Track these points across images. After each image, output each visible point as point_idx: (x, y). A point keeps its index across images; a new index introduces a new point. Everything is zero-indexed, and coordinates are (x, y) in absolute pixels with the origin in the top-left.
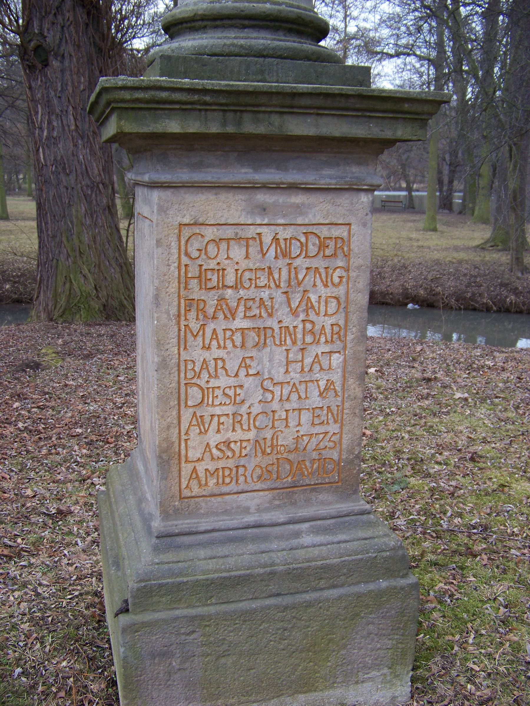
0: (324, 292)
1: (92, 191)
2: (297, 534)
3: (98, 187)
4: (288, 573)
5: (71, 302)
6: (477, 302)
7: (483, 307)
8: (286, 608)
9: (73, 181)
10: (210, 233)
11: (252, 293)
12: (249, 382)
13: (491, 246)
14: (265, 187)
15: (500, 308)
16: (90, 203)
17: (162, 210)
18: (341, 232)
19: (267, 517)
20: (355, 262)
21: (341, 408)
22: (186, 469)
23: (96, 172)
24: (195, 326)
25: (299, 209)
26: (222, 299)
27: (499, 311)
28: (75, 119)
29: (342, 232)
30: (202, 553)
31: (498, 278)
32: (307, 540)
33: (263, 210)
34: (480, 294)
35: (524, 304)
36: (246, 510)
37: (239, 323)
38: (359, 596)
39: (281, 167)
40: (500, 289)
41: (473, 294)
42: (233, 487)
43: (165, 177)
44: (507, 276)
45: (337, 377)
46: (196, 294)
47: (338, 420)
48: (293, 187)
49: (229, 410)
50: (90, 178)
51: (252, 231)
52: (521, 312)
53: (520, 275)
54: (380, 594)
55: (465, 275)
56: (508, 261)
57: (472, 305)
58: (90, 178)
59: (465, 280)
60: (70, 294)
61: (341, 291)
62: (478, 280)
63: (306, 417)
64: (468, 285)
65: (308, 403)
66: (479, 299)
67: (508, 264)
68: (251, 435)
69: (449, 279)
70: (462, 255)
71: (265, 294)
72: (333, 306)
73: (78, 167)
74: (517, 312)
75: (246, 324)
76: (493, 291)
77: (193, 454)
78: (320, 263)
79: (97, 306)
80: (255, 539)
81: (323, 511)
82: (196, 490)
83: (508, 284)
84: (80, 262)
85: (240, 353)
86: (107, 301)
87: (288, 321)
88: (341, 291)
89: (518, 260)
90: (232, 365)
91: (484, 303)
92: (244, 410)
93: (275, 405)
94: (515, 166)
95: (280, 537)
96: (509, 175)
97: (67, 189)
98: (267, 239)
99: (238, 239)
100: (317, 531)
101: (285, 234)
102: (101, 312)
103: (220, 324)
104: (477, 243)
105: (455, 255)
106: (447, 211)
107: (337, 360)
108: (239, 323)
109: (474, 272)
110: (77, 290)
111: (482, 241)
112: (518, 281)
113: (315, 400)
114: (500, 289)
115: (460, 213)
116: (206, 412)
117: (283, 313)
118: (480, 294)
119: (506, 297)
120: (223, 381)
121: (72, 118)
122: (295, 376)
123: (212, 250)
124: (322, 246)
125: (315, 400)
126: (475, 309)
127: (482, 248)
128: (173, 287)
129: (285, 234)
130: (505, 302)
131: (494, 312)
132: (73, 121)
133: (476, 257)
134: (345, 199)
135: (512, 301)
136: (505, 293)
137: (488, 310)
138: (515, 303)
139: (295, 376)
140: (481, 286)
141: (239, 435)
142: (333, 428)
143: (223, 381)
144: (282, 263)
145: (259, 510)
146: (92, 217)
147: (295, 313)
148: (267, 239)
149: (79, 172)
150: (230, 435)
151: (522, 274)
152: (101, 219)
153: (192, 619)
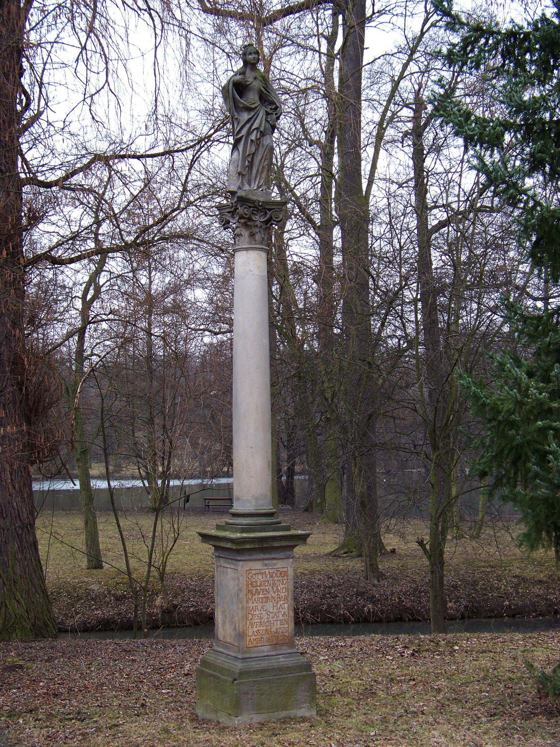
0: (282, 586)
1: (23, 531)
2: (279, 658)
3: (27, 527)
4: (278, 668)
5: (6, 623)
6: (334, 614)
7: (340, 619)
8: (278, 679)
9: (8, 524)
10: (253, 572)
11: (264, 587)
12: (264, 612)
13: (345, 553)
14: (267, 559)
15: (359, 619)
16: (21, 541)
17: (242, 567)
18: (285, 570)
19: (270, 654)
20: (289, 578)
21: (288, 619)
22: (248, 638)
23: (26, 515)
24: (250, 597)
25: (275, 564)
26: (257, 589)
27: (357, 622)
28: (11, 474)
29: (285, 570)
30: (254, 663)
31: (354, 587)
32: (282, 660)
33: (266, 565)
34: (336, 606)
35: (382, 612)
36: (264, 652)
37: (261, 596)
38: (299, 676)
39: (270, 554)
40: (356, 598)
41: (329, 606)
42: (260, 644)
43: (243, 558)
44: (362, 585)
45: (286, 610)
46: (250, 588)
47: (287, 623)
48: (274, 559)
49: (259, 621)
50: (21, 520)
51: (263, 571)
52: (380, 621)
53: (376, 582)
54: (304, 676)
55: (319, 586)
56: (363, 568)
57: (329, 617)
58: (21, 520)
59: (320, 592)
60: (6, 616)
61: (286, 586)
62: (333, 591)
63: (279, 622)
64: (323, 597)
65: (279, 619)
66: (336, 610)
67: (363, 571)
68: (265, 628)
69: (302, 592)
70: (314, 565)
71: (267, 588)
72: (284, 590)
73: (13, 512)
74: (376, 621)
75: (262, 596)
76: (350, 601)
77: (250, 634)
78: (280, 578)
79: (28, 626)
80: (267, 660)
81: (285, 652)
82: (251, 645)
83: (364, 593)
84: (14, 589)
85: (261, 604)
86: (35, 622)
87: (273, 595)
88: (286, 586)
89: (372, 567)
90: (259, 608)
91: (341, 614)
92: (262, 620)
93: (271, 619)
94: (360, 471)
95: (274, 659)
96: (355, 479)
97: (4, 530)
98: (267, 573)
99: (260, 573)
100: (284, 658)
101: (271, 571)
102: (32, 631)
103: (256, 596)
104: (329, 549)
105: (306, 565)
106: (289, 507)
107: (286, 605)
108: (261, 596)
109: (328, 583)
110: (12, 613)
111: (335, 547)
112: (374, 588)
113: (281, 618)
114: (356, 598)
115: (306, 510)
116: (253, 621)
117: (272, 593)
118: (336, 606)
119: (364, 606)
120: (257, 612)
121: (9, 473)
122: (275, 610)
123: (254, 576)
124: (281, 574)
125: (281, 618)
126: (332, 622)
127: (334, 555)
128: (245, 587)
129: (271, 571)
130: (363, 611)
131: (353, 623)
132: (9, 476)
133: (331, 566)
134: (286, 561)
135: (369, 610)
136: (362, 602)
137: (346, 621)
138: (373, 612)
139: (275, 610)
140: (337, 596)
141: (261, 628)
142: (286, 626)
143: (257, 612)
144: (271, 579)
145: (267, 652)
146: (23, 552)
147: (274, 592)
148: (267, 573)
149: (13, 515)
150: (259, 628)
151: (379, 581)
152: (29, 553)
153: (254, 681)
